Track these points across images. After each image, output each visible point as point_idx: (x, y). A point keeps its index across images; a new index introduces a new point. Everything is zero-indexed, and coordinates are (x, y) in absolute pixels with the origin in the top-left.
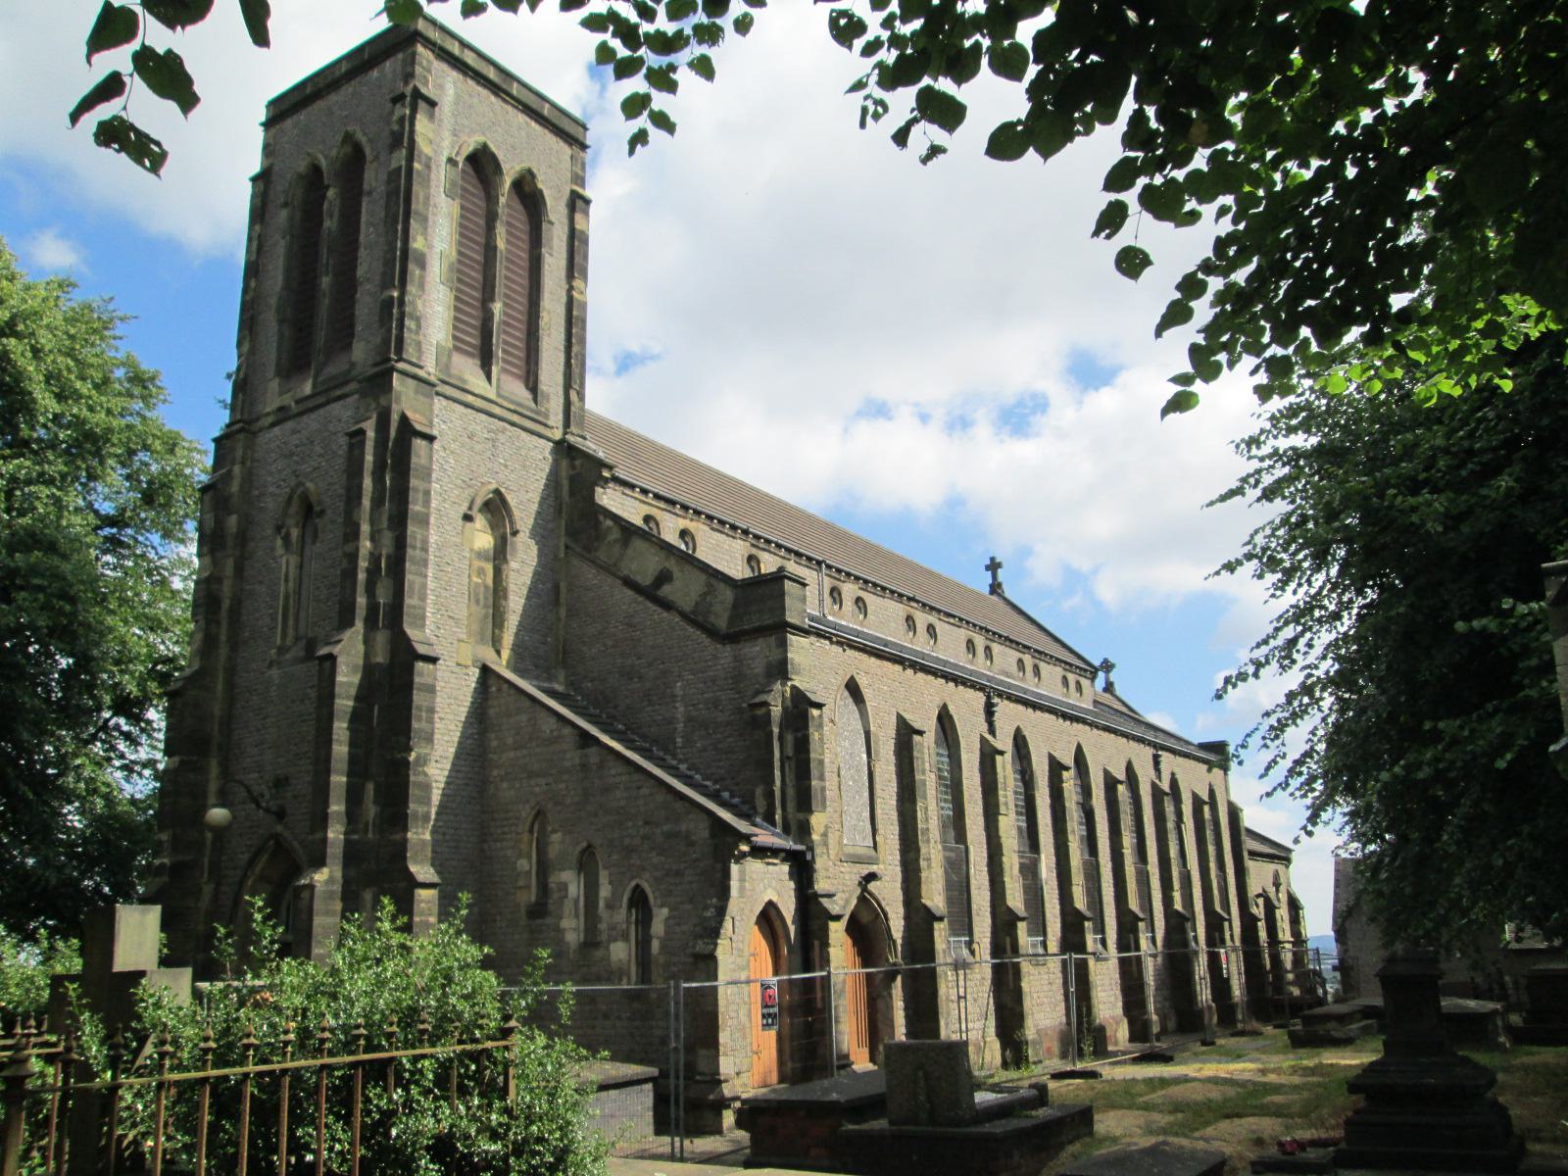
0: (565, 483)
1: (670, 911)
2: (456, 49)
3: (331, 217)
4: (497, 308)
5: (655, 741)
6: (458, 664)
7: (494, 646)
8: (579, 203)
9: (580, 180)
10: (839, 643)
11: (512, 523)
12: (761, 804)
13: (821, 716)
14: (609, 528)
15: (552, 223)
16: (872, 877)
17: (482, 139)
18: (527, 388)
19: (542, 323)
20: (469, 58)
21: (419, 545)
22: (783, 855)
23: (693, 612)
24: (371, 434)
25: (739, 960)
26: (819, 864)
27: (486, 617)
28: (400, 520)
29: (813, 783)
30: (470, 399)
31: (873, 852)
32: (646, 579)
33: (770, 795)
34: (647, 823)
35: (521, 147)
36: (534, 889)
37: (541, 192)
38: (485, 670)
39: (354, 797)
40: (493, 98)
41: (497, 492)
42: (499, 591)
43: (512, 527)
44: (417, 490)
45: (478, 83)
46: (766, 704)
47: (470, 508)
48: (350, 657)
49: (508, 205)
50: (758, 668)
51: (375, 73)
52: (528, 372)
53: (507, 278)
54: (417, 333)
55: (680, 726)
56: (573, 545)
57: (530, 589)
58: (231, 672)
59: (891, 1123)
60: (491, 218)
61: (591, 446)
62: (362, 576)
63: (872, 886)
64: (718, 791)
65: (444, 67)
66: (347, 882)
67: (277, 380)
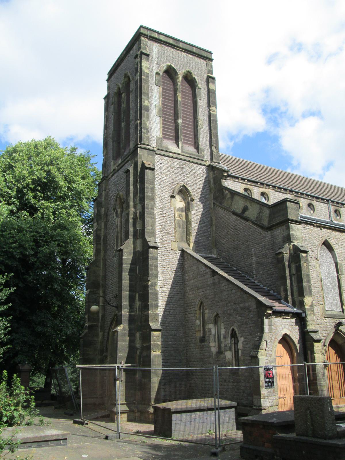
0: (212, 180)
1: (244, 339)
2: (156, 35)
3: (124, 103)
4: (180, 121)
5: (246, 273)
6: (172, 250)
7: (187, 242)
8: (210, 80)
9: (211, 72)
10: (317, 226)
11: (191, 196)
12: (283, 294)
13: (307, 256)
14: (227, 194)
15: (200, 89)
16: (340, 324)
17: (168, 64)
18: (195, 148)
19: (199, 124)
20: (162, 38)
21: (150, 207)
22: (291, 315)
23: (256, 221)
24: (132, 171)
25: (270, 358)
26: (309, 318)
27: (183, 232)
28: (142, 200)
29: (304, 284)
30: (171, 154)
31: (342, 313)
32: (239, 211)
33: (286, 290)
34: (235, 304)
35: (183, 64)
36: (202, 332)
37: (194, 78)
38: (183, 251)
39: (132, 299)
40: (172, 50)
41: (184, 186)
42: (188, 222)
43: (191, 199)
44: (148, 188)
45: (166, 45)
46: (281, 253)
47: (173, 193)
48: (128, 250)
49: (182, 85)
50: (280, 239)
51: (132, 52)
52: (195, 143)
53: (183, 110)
54: (147, 134)
55: (254, 266)
56: (216, 203)
57: (200, 221)
58: (105, 260)
59: (297, 435)
60: (175, 90)
61: (223, 166)
62: (131, 221)
63: (341, 328)
64: (269, 290)
65: (152, 42)
66: (130, 330)
67: (113, 161)
